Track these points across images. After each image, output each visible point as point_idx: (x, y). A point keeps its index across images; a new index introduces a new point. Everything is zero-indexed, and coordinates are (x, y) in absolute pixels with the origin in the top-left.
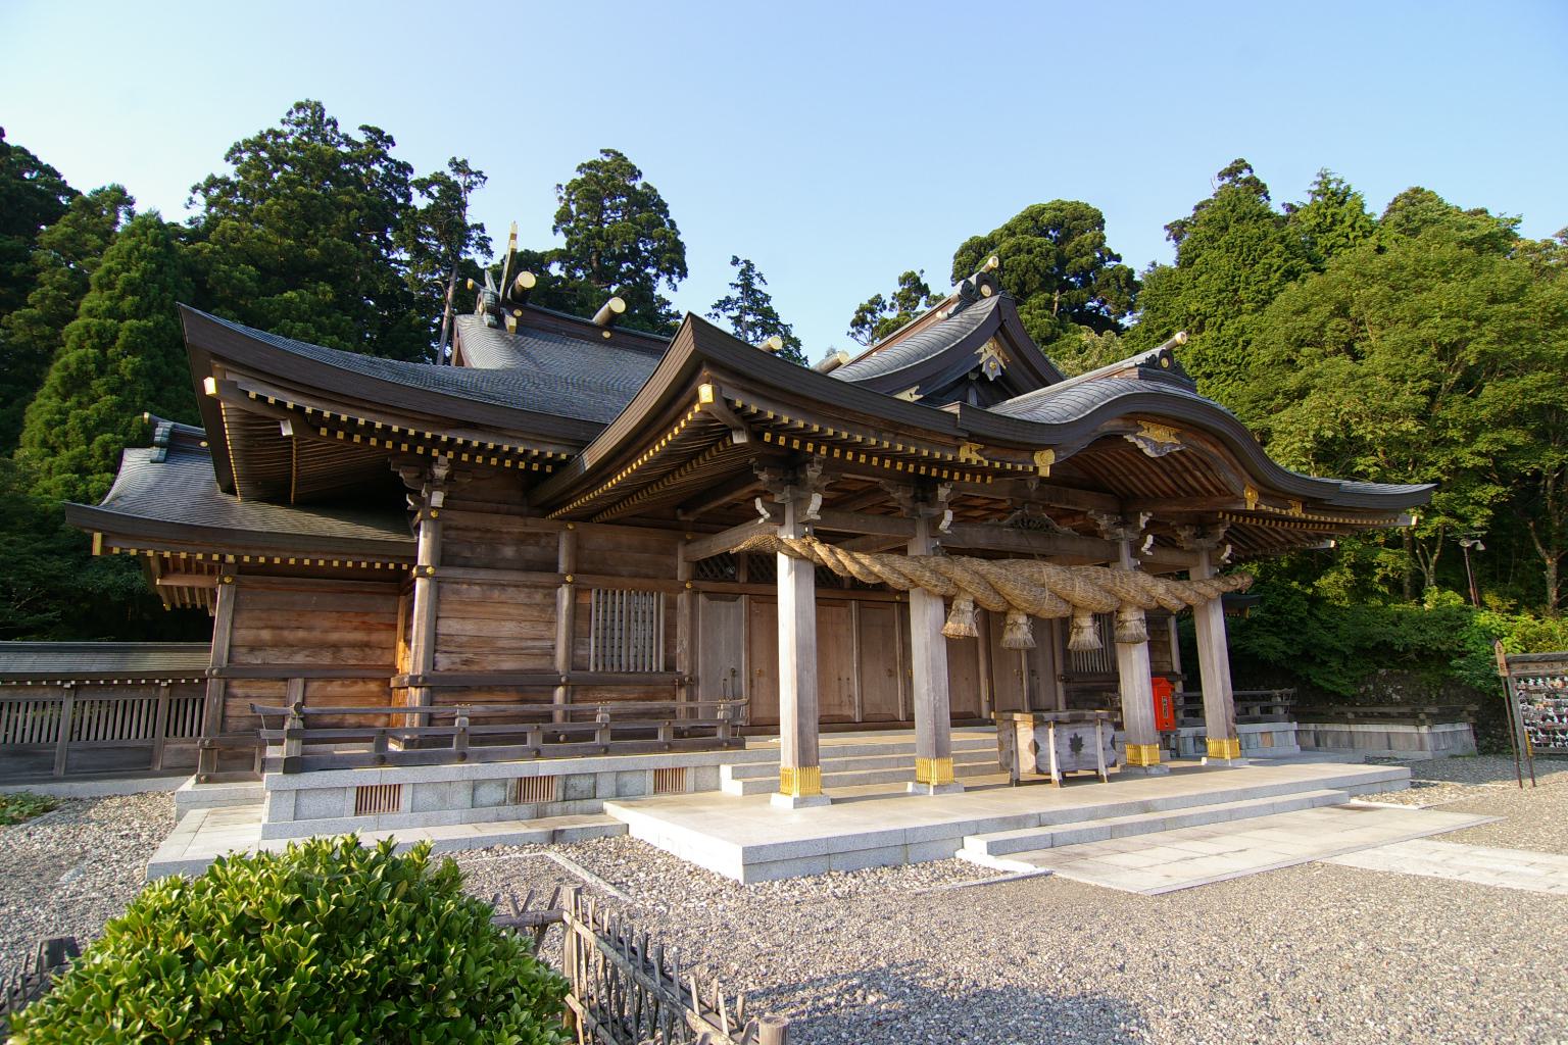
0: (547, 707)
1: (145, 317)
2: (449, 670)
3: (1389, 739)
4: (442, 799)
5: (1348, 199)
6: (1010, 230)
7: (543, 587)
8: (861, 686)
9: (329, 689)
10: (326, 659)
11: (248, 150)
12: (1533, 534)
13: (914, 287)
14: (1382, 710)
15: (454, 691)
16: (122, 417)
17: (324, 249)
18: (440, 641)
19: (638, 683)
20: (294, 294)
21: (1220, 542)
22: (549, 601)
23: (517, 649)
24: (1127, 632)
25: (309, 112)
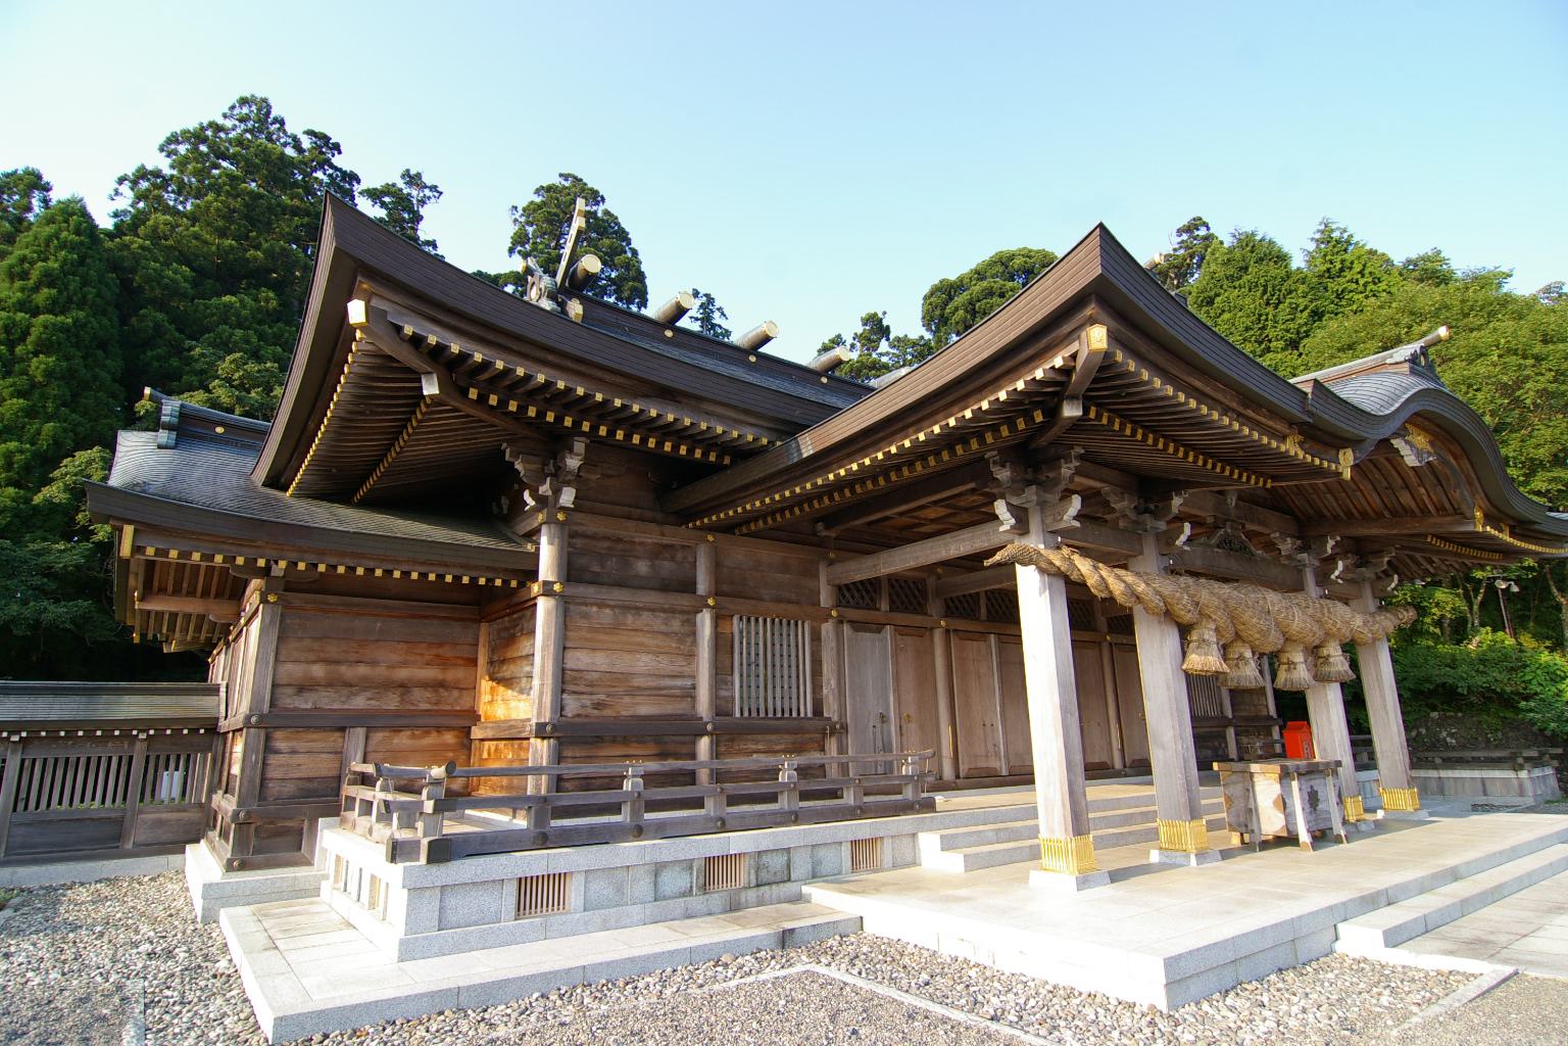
0: (687, 764)
1: (63, 313)
2: (579, 715)
3: (1484, 785)
4: (619, 889)
5: (1351, 248)
6: (979, 274)
7: (682, 612)
8: (1005, 733)
9: (395, 741)
10: (392, 702)
11: (188, 140)
12: (1549, 576)
13: (876, 328)
14: (1475, 754)
15: (586, 743)
16: (31, 424)
17: (269, 253)
18: (567, 678)
19: (788, 732)
20: (234, 299)
21: (1384, 572)
22: (687, 629)
23: (655, 688)
24: (1333, 669)
25: (254, 108)
